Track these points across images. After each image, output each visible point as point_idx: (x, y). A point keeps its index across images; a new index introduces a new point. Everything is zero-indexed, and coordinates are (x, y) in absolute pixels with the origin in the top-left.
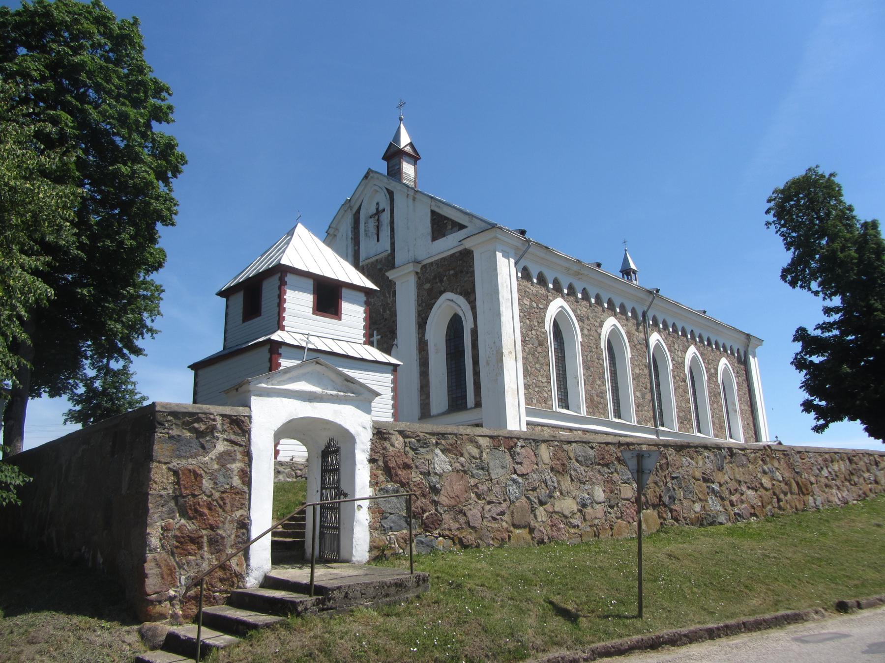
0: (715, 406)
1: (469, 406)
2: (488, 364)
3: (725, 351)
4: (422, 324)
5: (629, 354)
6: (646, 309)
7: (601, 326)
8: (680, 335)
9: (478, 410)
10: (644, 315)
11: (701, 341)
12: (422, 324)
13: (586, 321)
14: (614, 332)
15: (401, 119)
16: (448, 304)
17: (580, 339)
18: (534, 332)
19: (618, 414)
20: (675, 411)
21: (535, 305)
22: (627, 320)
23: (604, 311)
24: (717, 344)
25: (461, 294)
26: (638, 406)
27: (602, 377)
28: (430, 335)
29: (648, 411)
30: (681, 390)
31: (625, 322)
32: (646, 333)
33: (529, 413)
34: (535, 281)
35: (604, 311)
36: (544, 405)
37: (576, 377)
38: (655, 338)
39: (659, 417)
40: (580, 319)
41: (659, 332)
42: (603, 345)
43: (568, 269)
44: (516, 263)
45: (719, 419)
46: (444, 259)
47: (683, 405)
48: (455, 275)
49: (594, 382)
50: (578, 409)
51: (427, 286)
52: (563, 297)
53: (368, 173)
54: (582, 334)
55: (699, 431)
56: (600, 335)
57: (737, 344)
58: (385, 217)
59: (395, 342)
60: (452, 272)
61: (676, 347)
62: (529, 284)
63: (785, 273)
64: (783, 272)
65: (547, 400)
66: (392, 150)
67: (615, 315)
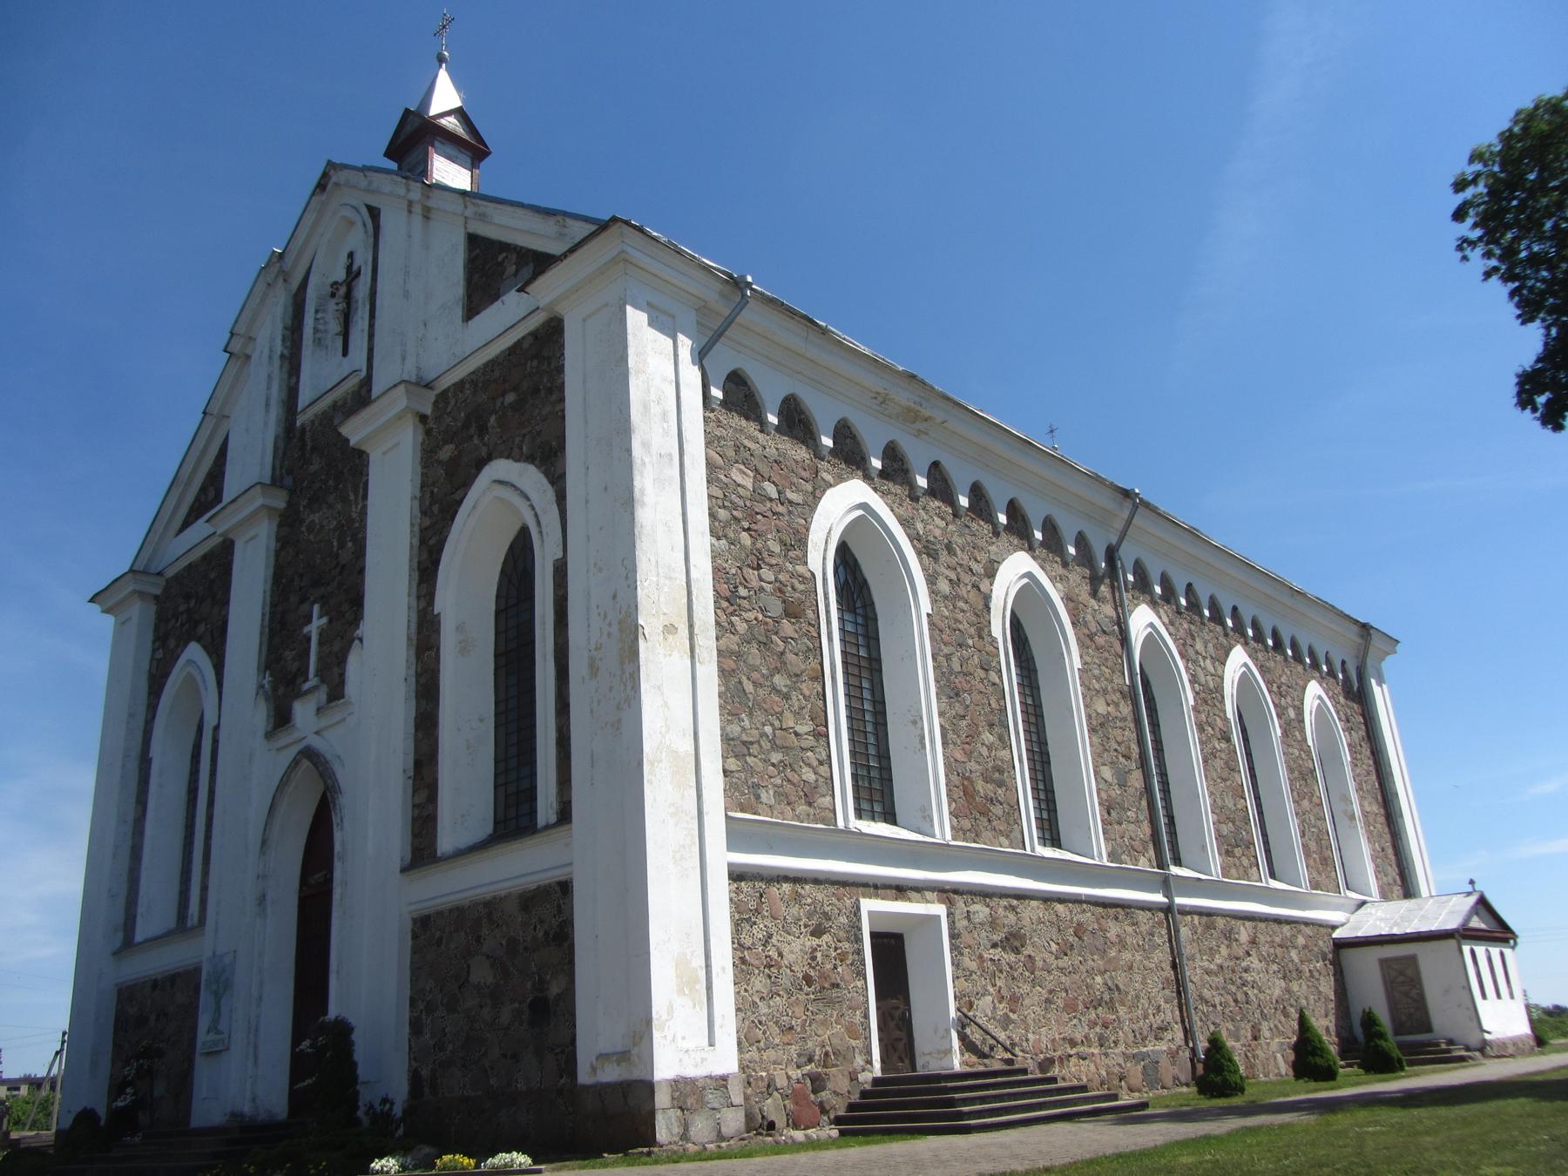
0: (1305, 803)
1: (541, 821)
2: (594, 670)
3: (1315, 665)
4: (426, 570)
5: (1074, 659)
6: (1114, 541)
7: (991, 574)
8: (1205, 616)
9: (561, 832)
10: (1111, 554)
11: (1259, 637)
12: (426, 570)
13: (944, 556)
14: (1029, 593)
15: (441, 60)
16: (502, 493)
17: (926, 606)
18: (767, 574)
19: (1051, 835)
20: (1208, 820)
21: (772, 491)
22: (1065, 565)
23: (996, 534)
24: (1294, 645)
25: (530, 459)
26: (1108, 807)
27: (998, 722)
28: (446, 600)
29: (1137, 822)
30: (1219, 763)
31: (1061, 571)
32: (1118, 605)
33: (737, 836)
34: (773, 419)
35: (996, 534)
36: (802, 808)
37: (916, 721)
38: (1142, 619)
39: (1165, 842)
40: (927, 550)
41: (1153, 604)
42: (999, 627)
43: (883, 400)
44: (700, 357)
45: (1319, 841)
46: (491, 365)
47: (1229, 803)
48: (517, 407)
49: (972, 736)
50: (923, 822)
51: (446, 452)
52: (867, 478)
53: (325, 175)
54: (933, 592)
55: (1273, 875)
56: (987, 598)
57: (1340, 649)
58: (361, 289)
59: (358, 632)
60: (510, 398)
61: (1199, 646)
62: (752, 427)
63: (1527, 386)
64: (1520, 384)
65: (813, 794)
66: (409, 129)
67: (1030, 549)
